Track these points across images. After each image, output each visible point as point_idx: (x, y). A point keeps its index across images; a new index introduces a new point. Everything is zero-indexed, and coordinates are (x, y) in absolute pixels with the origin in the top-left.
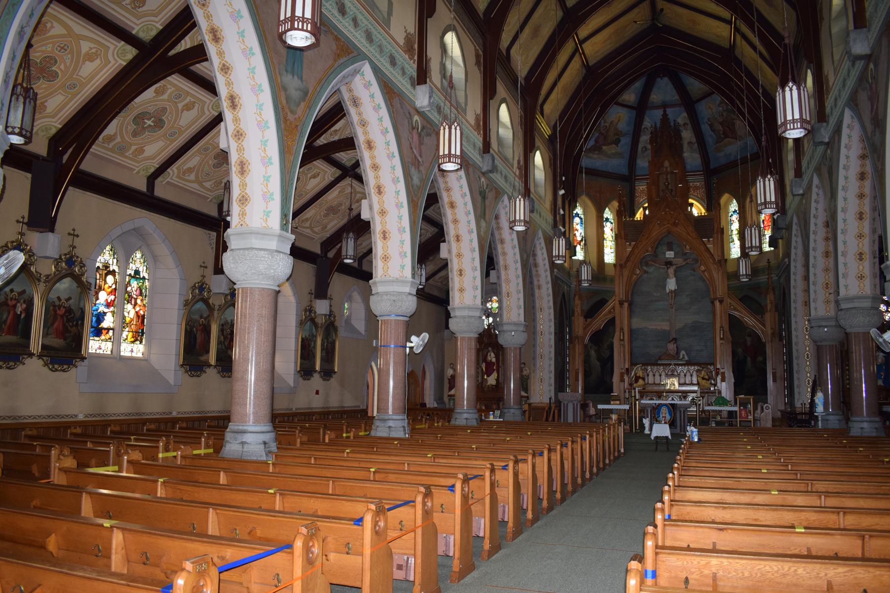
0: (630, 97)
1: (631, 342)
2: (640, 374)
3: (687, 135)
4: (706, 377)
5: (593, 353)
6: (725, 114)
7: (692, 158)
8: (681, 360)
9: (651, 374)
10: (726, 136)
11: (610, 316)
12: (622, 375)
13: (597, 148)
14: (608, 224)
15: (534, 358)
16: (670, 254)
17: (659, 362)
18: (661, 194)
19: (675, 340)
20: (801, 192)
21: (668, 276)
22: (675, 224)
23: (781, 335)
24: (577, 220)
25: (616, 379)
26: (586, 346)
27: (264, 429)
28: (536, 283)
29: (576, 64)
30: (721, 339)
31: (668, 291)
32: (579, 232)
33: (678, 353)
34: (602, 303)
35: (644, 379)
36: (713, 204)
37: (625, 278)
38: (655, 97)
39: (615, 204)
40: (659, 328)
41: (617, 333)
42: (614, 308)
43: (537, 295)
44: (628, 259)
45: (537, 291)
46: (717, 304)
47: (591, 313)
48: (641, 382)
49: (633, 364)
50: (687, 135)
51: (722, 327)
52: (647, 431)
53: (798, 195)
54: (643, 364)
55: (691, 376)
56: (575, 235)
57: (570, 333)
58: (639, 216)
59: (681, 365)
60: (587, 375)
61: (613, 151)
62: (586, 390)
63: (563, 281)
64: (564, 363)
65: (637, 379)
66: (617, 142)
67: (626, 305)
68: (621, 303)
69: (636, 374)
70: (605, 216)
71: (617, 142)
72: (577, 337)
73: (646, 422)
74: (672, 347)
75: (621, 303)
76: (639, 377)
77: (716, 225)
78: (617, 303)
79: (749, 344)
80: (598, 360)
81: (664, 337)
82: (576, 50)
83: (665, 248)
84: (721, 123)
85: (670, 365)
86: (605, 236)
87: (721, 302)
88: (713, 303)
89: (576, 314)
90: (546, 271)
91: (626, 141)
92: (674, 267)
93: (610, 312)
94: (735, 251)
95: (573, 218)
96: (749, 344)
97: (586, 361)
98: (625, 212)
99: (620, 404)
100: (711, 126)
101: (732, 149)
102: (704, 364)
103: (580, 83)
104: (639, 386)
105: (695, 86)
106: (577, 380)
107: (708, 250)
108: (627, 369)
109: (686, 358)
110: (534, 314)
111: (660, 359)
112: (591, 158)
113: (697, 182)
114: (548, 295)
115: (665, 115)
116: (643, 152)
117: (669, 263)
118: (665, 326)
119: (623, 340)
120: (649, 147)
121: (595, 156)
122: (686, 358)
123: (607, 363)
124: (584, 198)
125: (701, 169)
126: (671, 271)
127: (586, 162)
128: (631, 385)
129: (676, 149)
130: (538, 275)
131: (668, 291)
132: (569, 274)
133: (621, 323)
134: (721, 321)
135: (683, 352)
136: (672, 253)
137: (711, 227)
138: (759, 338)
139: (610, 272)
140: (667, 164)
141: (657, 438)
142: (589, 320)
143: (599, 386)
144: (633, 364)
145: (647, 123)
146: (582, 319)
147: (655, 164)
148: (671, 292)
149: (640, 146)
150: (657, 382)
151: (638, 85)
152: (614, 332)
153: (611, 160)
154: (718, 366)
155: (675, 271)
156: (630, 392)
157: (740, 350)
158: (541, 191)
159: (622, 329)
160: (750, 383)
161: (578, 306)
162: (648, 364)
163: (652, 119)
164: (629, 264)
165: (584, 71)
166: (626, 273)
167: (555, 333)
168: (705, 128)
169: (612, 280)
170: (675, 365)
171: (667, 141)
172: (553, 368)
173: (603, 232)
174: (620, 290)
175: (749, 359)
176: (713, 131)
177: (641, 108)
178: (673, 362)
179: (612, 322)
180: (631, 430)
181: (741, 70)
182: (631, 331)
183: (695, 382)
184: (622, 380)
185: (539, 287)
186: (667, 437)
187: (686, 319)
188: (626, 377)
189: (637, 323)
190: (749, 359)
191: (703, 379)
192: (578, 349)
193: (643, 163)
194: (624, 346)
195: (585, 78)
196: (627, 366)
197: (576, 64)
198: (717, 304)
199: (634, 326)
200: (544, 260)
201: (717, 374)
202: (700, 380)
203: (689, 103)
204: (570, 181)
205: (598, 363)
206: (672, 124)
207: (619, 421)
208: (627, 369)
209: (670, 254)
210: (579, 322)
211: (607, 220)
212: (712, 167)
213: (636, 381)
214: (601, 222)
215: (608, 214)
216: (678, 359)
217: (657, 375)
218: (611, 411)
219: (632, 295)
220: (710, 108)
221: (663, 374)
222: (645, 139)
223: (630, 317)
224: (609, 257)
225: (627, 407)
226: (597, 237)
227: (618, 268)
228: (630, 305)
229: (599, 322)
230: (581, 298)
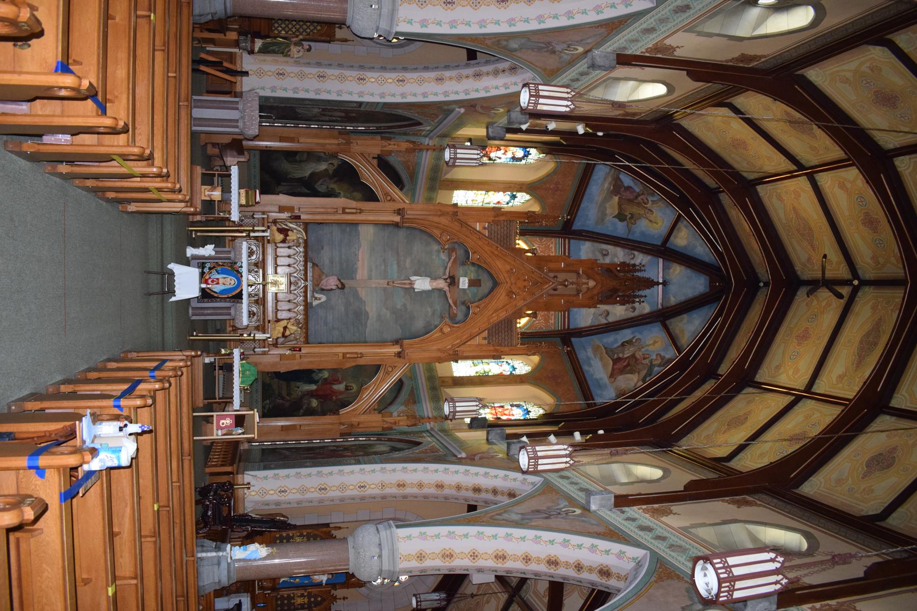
0: (685, 238)
1: (339, 223)
2: (292, 236)
3: (619, 312)
4: (287, 333)
5: (323, 166)
6: (647, 361)
7: (585, 317)
8: (313, 296)
9: (291, 252)
10: (616, 361)
11: (380, 194)
12: (290, 209)
13: (617, 188)
14: (508, 198)
15: (319, 64)
16: (464, 283)
17: (309, 265)
18: (552, 275)
19: (343, 287)
20: (593, 507)
21: (434, 278)
22: (510, 293)
23: (350, 434)
24: (520, 153)
25: (284, 199)
26: (334, 156)
27: (229, 11)
28: (447, 74)
29: (767, 159)
30: (344, 354)
31: (413, 278)
32: (502, 156)
33: (322, 290)
34: (398, 181)
35: (284, 241)
36: (531, 341)
37: (436, 219)
38: (678, 271)
39: (536, 208)
40: (360, 264)
41: (353, 204)
42: (392, 200)
43: (426, 75)
44: (463, 224)
45: (433, 75)
46: (397, 349)
47: (384, 166)
48: (280, 237)
49: (306, 225)
50: (619, 312)
51: (362, 355)
52: (190, 251)
53: (589, 502)
54: (306, 242)
55: (289, 310)
56: (499, 149)
57: (355, 132)
58: (522, 244)
59: (306, 296)
60: (290, 155)
61: (608, 211)
62: (266, 154)
63: (440, 123)
64: (308, 119)
65: (284, 232)
66: (621, 217)
67: (397, 219)
68: (399, 212)
69: (292, 230)
70: (519, 195)
71: (621, 217)
72: (349, 143)
73: (208, 250)
74: (331, 282)
75: (399, 212)
76: (287, 235)
77: (506, 349)
78: (401, 206)
79: (336, 387)
80: (312, 174)
81: (347, 272)
82: (800, 166)
83: (473, 276)
84: (633, 356)
85: (306, 280)
86: (491, 193)
87: (399, 355)
88: (397, 342)
89: (384, 143)
90: (467, 92)
91: (620, 229)
92: (446, 288)
93: (387, 194)
94: (462, 369)
95: (525, 148)
96: (336, 387)
97: (311, 156)
98: (529, 225)
99: (241, 206)
100: (630, 342)
101: (597, 369)
102: (307, 329)
103: (729, 166)
104: (272, 234)
105: (690, 327)
106: (282, 139)
107: (472, 337)
108: (298, 217)
109: (315, 303)
110: (394, 69)
111: (314, 265)
112: (605, 179)
113: (552, 321)
114: (425, 95)
115: (658, 284)
116: (601, 251)
117: (453, 281)
118: (362, 273)
119: (344, 212)
120: (607, 260)
121: (606, 185)
122: (315, 303)
123: (308, 187)
124: (550, 166)
125: (571, 327)
126: (442, 284)
127: (602, 173)
128: (275, 222)
129: (610, 297)
130: (459, 78)
131: (413, 278)
132: (444, 136)
133: (370, 211)
134: (370, 354)
135: (323, 298)
136: (466, 287)
137: (500, 341)
138: (345, 404)
139: (441, 197)
140: (592, 283)
141: (172, 274)
142: (375, 162)
143: (271, 174)
144: (306, 225)
145: (640, 258)
146: (376, 151)
147: (591, 268)
148: (412, 283)
149: (610, 248)
150: (280, 261)
151: (702, 250)
152: (354, 199)
153: (599, 207)
154: (304, 351)
155: (440, 290)
156: (262, 222)
157: (326, 375)
158: (598, 94)
159: (361, 211)
160: (280, 392)
161: (396, 148)
162: (306, 247)
163: (655, 269)
164: (456, 226)
165: (751, 176)
166: (444, 221)
167: (360, 104)
168: (626, 334)
169: (430, 200)
170: (306, 287)
171: (622, 284)
172: (301, 95)
173: (497, 190)
174: (416, 209)
175: (313, 387)
176: (623, 345)
177: (665, 251)
178: (309, 283)
179: (370, 196)
180: (193, 224)
181: (832, 438)
182: (354, 224)
183: (281, 315)
184: (282, 209)
185: (440, 80)
186: (172, 292)
187: (373, 306)
188: (285, 215)
189: (367, 233)
190: (313, 387)
191: (285, 328)
192: (331, 144)
193: (586, 250)
194: (336, 213)
195: (737, 175)
196: (303, 217)
197: (775, 162)
198: (397, 349)
199: (362, 229)
200: (486, 89)
201: (293, 349)
202: (284, 323)
203: (663, 316)
204: (600, 143)
205: (307, 174)
206: (641, 293)
207: (486, 155)
208: (298, 217)
209: (464, 283)
210: (375, 146)
211: (514, 197)
212: (573, 340)
213: (281, 231)
214: (513, 188)
215: (522, 198)
216: (314, 291)
217: (291, 261)
218: (226, 190)
219: (408, 228)
220: (655, 342)
221: (292, 270)
222: (619, 255)
223: (376, 224)
224: (462, 198)
225: (235, 216)
226: (495, 182)
227: (451, 209)
228: (396, 225)
229: (371, 176)
230: (408, 151)
